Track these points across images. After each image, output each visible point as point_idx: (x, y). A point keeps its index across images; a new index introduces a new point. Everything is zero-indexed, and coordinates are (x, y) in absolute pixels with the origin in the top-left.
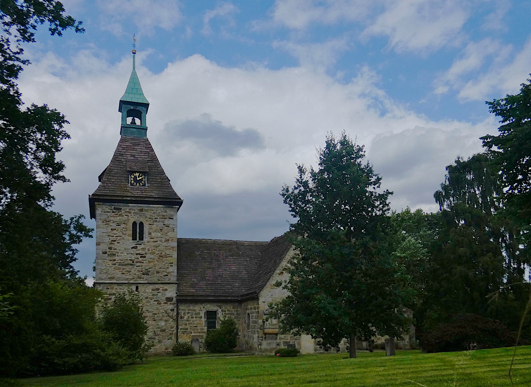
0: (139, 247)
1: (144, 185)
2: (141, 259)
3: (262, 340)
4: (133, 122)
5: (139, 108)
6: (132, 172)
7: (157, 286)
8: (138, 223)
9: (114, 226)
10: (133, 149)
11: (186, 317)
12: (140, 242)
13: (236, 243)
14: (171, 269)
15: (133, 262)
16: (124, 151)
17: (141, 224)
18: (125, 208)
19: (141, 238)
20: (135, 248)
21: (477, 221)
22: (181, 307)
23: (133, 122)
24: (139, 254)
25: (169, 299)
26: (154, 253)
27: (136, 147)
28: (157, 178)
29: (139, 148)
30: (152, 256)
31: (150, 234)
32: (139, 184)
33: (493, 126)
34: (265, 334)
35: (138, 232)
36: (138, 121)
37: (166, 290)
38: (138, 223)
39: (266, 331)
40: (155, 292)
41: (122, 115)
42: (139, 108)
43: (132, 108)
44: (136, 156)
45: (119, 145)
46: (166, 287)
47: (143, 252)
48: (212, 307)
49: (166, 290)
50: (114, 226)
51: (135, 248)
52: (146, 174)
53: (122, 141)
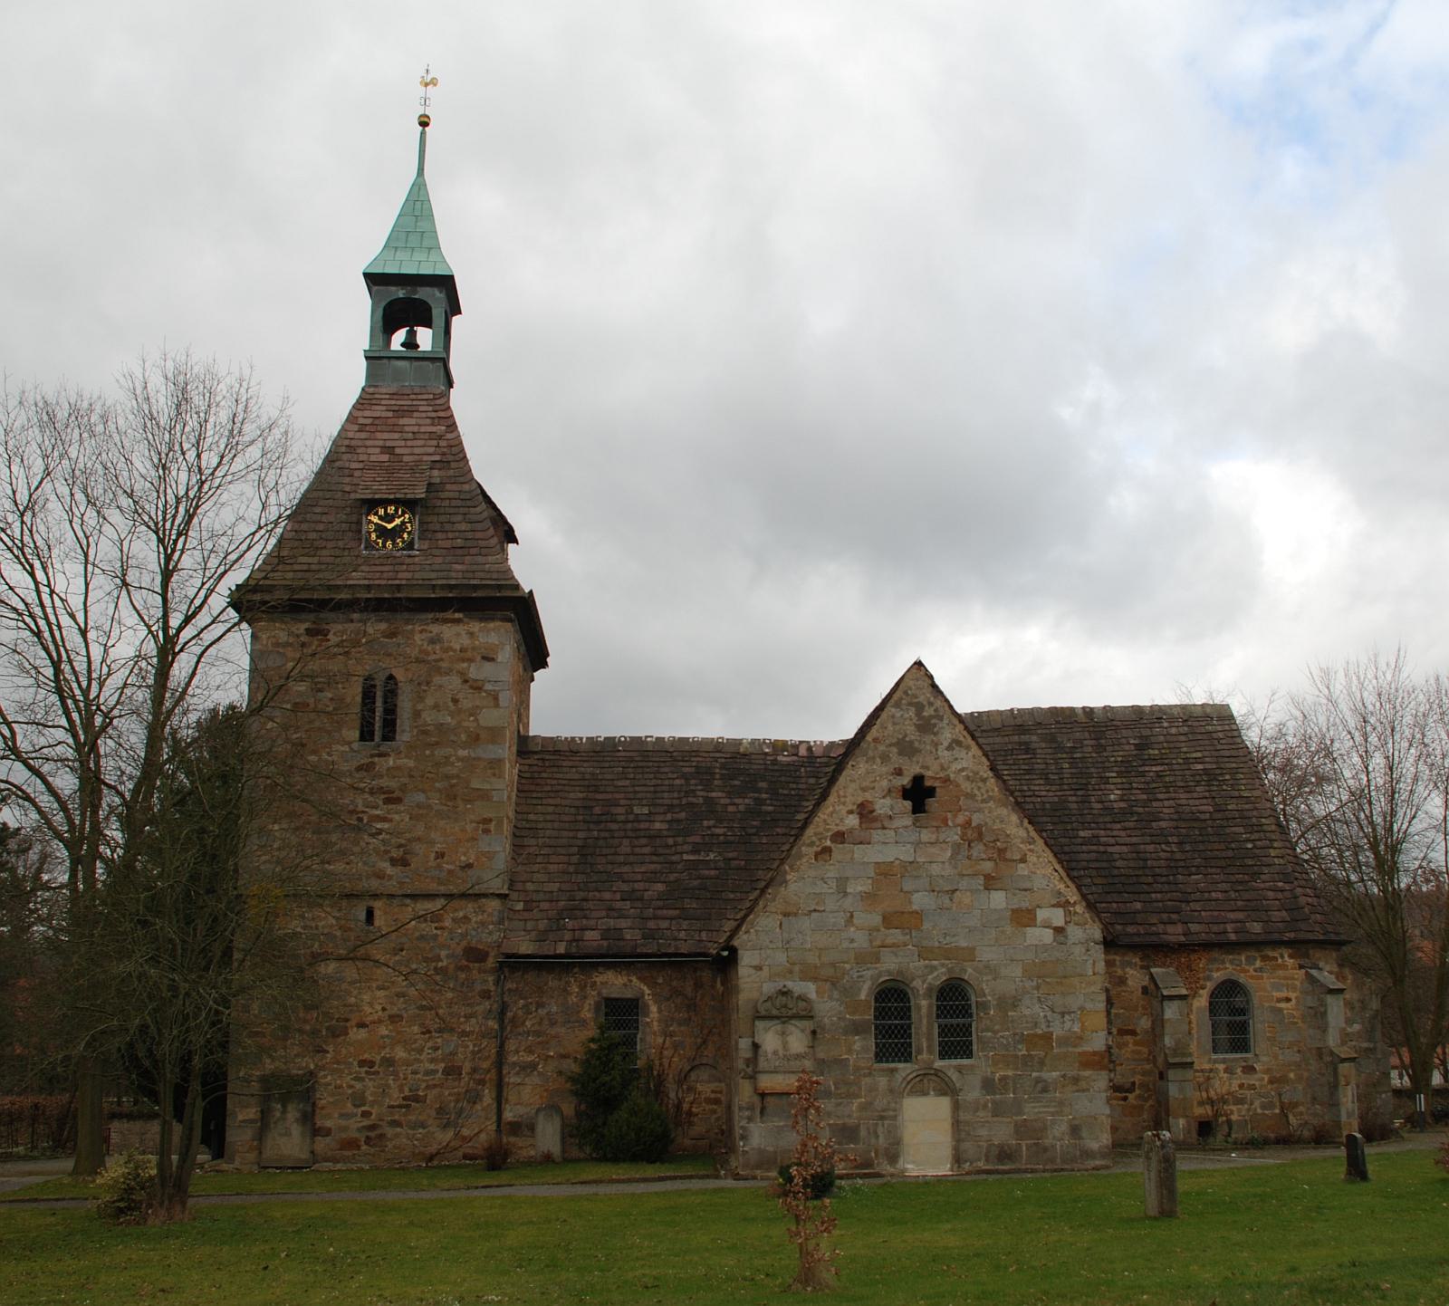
1: (410, 546)
3: (750, 1119)
4: (410, 343)
5: (423, 293)
6: (371, 505)
8: (379, 682)
10: (394, 428)
12: (386, 747)
13: (1062, 719)
15: (360, 820)
16: (363, 435)
18: (339, 630)
20: (367, 768)
23: (410, 343)
24: (381, 790)
27: (402, 421)
28: (455, 518)
29: (413, 421)
31: (417, 714)
32: (394, 543)
34: (763, 1095)
36: (425, 338)
38: (379, 682)
39: (766, 1082)
42: (423, 293)
43: (401, 293)
44: (398, 451)
45: (351, 418)
47: (393, 784)
48: (615, 983)
52: (419, 509)
53: (364, 401)
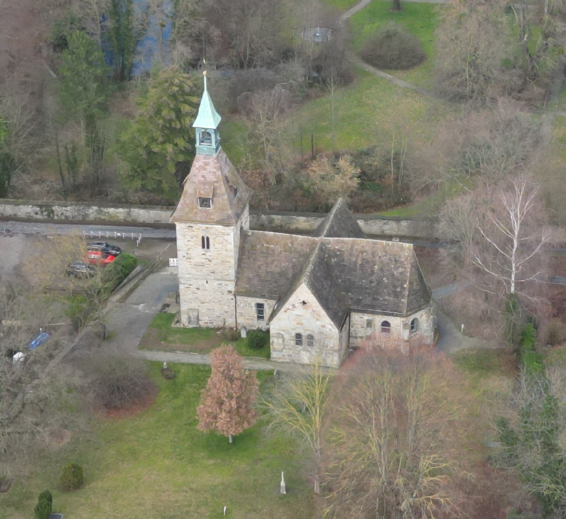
0: (208, 254)
2: (209, 263)
7: (220, 282)
9: (189, 239)
10: (205, 169)
11: (241, 306)
14: (230, 271)
17: (208, 239)
19: (208, 247)
21: (233, 84)
22: (238, 298)
25: (230, 292)
26: (217, 259)
30: (216, 261)
33: (136, 24)
35: (206, 243)
37: (227, 285)
40: (219, 286)
41: (358, 311)
46: (228, 283)
48: (260, 301)
49: (227, 285)
50: (189, 239)
51: (204, 254)
